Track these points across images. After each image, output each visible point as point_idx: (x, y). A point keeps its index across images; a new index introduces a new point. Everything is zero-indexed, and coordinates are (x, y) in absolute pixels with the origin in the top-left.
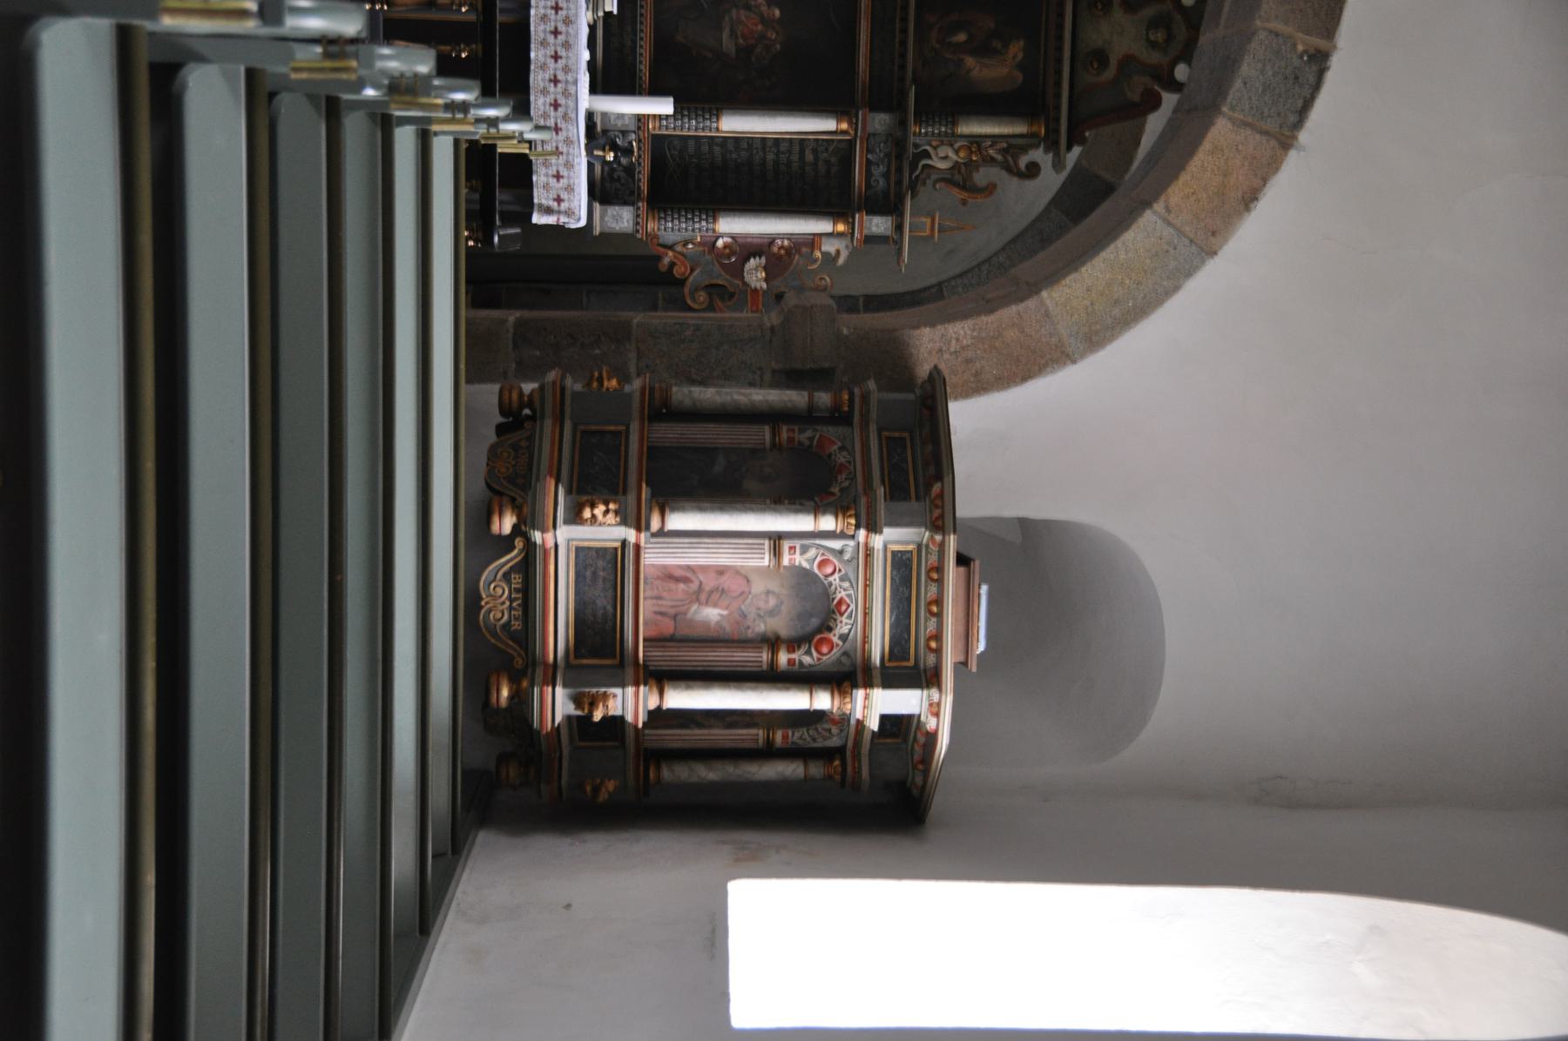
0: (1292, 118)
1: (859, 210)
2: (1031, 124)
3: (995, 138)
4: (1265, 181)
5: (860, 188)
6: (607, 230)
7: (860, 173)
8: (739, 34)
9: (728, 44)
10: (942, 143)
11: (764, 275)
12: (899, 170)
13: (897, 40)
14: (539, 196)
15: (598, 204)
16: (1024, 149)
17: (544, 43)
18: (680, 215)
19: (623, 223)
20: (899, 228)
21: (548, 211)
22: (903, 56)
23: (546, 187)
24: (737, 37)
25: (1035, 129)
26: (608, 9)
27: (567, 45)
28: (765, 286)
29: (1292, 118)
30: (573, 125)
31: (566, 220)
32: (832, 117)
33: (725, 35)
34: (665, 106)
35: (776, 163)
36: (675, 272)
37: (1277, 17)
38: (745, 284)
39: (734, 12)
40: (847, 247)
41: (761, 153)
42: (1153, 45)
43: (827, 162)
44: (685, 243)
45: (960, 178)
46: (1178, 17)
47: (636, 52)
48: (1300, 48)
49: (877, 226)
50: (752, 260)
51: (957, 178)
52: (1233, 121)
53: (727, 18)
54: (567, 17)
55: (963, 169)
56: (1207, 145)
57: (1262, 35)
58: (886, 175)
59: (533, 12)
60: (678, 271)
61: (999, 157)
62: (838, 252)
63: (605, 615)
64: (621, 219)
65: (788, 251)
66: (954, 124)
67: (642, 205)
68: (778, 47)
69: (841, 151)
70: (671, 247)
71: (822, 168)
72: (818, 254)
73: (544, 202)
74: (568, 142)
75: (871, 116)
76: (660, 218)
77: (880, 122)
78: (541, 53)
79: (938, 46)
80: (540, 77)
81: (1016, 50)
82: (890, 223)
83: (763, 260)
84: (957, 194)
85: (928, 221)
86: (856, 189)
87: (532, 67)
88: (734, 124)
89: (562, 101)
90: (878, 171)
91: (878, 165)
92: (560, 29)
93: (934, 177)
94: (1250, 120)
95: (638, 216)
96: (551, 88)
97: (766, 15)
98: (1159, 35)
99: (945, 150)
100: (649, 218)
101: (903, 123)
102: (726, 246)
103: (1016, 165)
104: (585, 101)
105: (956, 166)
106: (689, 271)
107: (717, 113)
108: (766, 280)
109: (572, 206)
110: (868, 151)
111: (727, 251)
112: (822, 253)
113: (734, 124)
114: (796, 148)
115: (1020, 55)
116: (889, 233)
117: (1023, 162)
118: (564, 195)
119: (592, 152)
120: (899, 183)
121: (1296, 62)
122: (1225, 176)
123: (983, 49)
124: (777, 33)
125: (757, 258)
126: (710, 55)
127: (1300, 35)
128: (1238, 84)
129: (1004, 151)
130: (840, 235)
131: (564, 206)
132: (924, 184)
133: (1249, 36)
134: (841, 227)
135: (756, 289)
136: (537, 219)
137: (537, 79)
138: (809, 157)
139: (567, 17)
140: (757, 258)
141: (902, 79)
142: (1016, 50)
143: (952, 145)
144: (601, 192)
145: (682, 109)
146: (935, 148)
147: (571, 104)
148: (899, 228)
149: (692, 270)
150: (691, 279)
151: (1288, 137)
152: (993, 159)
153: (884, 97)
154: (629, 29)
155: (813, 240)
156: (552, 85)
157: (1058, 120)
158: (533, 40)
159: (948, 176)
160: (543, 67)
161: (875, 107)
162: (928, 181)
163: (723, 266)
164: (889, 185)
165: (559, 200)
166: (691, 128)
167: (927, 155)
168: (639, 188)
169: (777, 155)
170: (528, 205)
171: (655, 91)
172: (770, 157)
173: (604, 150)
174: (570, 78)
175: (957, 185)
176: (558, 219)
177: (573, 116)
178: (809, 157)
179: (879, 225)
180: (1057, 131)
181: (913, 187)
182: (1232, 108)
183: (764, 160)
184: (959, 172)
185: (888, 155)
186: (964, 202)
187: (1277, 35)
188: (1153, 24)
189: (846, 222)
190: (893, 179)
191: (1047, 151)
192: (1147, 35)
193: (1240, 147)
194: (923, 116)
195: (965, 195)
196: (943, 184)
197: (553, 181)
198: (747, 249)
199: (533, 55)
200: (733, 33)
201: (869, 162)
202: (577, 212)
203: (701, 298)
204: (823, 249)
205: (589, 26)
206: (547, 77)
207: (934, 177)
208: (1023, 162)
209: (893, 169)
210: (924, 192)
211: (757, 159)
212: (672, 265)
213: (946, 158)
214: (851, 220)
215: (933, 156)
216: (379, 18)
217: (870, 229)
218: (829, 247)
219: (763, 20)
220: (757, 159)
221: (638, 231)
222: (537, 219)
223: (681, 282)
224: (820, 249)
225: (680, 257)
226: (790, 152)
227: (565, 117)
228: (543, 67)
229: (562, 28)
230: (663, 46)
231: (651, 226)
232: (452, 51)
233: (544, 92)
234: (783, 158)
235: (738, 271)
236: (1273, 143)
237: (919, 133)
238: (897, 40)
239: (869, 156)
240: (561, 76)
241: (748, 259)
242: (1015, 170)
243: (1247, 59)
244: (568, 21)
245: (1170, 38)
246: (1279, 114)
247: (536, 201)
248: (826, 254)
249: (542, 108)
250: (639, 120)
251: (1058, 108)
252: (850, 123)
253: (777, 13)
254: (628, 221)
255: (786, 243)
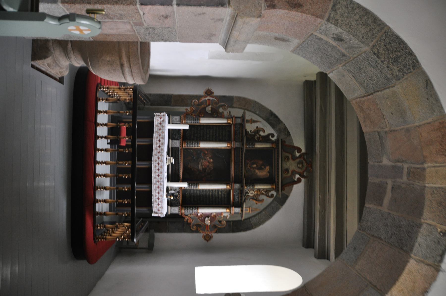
0: (439, 258)
1: (232, 206)
2: (272, 186)
3: (263, 189)
4: (430, 284)
5: (232, 201)
6: (172, 213)
7: (232, 197)
8: (203, 165)
9: (200, 168)
10: (251, 190)
11: (209, 222)
12: (241, 197)
13: (240, 167)
14: (154, 209)
15: (169, 207)
16: (270, 191)
17: (155, 172)
18: (189, 208)
19: (175, 211)
20: (242, 211)
21: (156, 213)
22: (242, 170)
23: (156, 207)
24: (202, 166)
25: (273, 187)
26: (172, 162)
27: (161, 173)
28: (210, 224)
29: (439, 258)
30: (162, 192)
31: (161, 215)
32: (225, 185)
33: (200, 166)
34: (184, 185)
35: (212, 195)
36: (188, 221)
37: (430, 218)
38: (205, 224)
39: (202, 161)
40: (229, 214)
41: (208, 193)
42: (299, 168)
43: (224, 194)
44: (191, 215)
45: (255, 198)
46: (304, 161)
47: (179, 161)
48: (439, 230)
49: (237, 210)
50: (207, 218)
51: (255, 198)
52: (415, 260)
53: (200, 162)
54: (161, 166)
55: (256, 196)
56: (406, 271)
57: (425, 226)
58: (238, 198)
59: (153, 165)
60: (189, 221)
61: (264, 193)
62: (227, 216)
63: (184, 142)
64: (175, 210)
65: (215, 216)
66: (254, 186)
67: (180, 207)
68: (212, 168)
69: (228, 192)
70: (187, 216)
71: (223, 195)
72: (222, 216)
73: (155, 211)
74: (161, 196)
75: (234, 185)
76: (184, 209)
77: (237, 186)
78: (155, 175)
79: (249, 168)
80: (154, 181)
81: (268, 168)
82: (239, 210)
83: (209, 218)
84: (254, 202)
85: (249, 209)
86: (231, 202)
87: (152, 178)
88: (202, 187)
89: (160, 186)
90: (236, 197)
91: (236, 196)
92: (159, 169)
93: (249, 198)
94: (422, 259)
95: (179, 209)
96: (157, 183)
97: (209, 161)
98: (300, 165)
99: (252, 192)
100: (182, 210)
101: (242, 186)
102: (200, 215)
103: (268, 194)
104: (166, 184)
105: (254, 195)
106: (192, 221)
107: (198, 184)
108: (210, 223)
109: (162, 212)
110: (234, 192)
111: (201, 216)
112: (224, 216)
113: (202, 187)
114: (217, 191)
115: (269, 169)
116: (239, 212)
117: (270, 194)
118: (160, 209)
119: (168, 197)
120: (241, 199)
121: (438, 236)
122: (414, 282)
123: (260, 169)
124: (212, 165)
125: (208, 218)
126: (196, 170)
127: (439, 225)
128: (417, 245)
129: (266, 192)
130: (227, 212)
131: (160, 212)
132: (247, 199)
133: (419, 226)
134: (228, 210)
135: (208, 225)
136: (153, 215)
137: (154, 181)
138: (220, 193)
139: (161, 166)
140: (208, 218)
141: (242, 176)
142: (268, 168)
143: (253, 191)
144: (170, 204)
145: (190, 184)
146: (249, 191)
147: (162, 187)
148: (242, 211)
149: (192, 221)
150: (192, 223)
151: (437, 266)
152: (263, 194)
153: (237, 180)
154: (177, 165)
155: (221, 214)
156: (157, 182)
157: (278, 185)
158: (153, 171)
159: (253, 197)
160: (155, 178)
161: (236, 182)
162: (248, 199)
163: (200, 220)
164: (239, 199)
165: (159, 210)
166: (192, 188)
167: (248, 193)
168: (180, 202)
169: (212, 193)
170: (151, 211)
171: (183, 181)
172: (211, 193)
173: (170, 196)
174: (162, 181)
175: (255, 200)
176: (159, 215)
177: (162, 190)
178: (220, 193)
179: (237, 210)
180: (278, 187)
181: (245, 201)
182: (415, 255)
183: (209, 194)
184: (255, 196)
185: (239, 193)
186: (257, 204)
187: (430, 225)
188: (299, 163)
189: (229, 209)
190: (240, 199)
191: (275, 191)
192: (298, 165)
193: (420, 271)
194: (248, 184)
195: (257, 202)
196: (252, 200)
197: (157, 206)
198: (206, 216)
199: (153, 175)
200: (202, 165)
201: (234, 195)
202: (163, 213)
203: (195, 228)
204: (224, 215)
205: (167, 166)
206: (156, 180)
207: (249, 198)
208: (270, 194)
209: (240, 196)
210: (247, 201)
211: (208, 194)
212: (188, 219)
213: (252, 193)
214: (230, 209)
215: (249, 193)
216: (115, 167)
217: (235, 211)
218: (225, 215)
219: (208, 162)
220: (208, 194)
221: (179, 213)
222: (153, 215)
223: (190, 224)
224: (223, 215)
225: (190, 218)
226: (215, 192)
227: (161, 190)
228: (155, 178)
229: (160, 168)
230: (185, 169)
231: (183, 211)
232: (123, 189)
233: (155, 184)
234: (214, 194)
235: (203, 221)
236: (433, 269)
237: (246, 188)
238: (240, 167)
239: (234, 193)
240: (159, 180)
241: (205, 218)
242: (268, 196)
243: (420, 235)
244: (161, 167)
245: (303, 166)
246: (433, 257)
247: (153, 210)
248: (224, 216)
249: (155, 188)
250: (179, 189)
251: (278, 182)
252: (230, 186)
253: (212, 160)
254: (177, 211)
255: (215, 214)
